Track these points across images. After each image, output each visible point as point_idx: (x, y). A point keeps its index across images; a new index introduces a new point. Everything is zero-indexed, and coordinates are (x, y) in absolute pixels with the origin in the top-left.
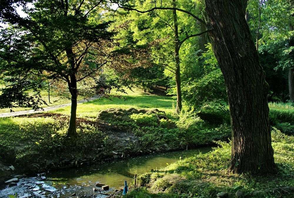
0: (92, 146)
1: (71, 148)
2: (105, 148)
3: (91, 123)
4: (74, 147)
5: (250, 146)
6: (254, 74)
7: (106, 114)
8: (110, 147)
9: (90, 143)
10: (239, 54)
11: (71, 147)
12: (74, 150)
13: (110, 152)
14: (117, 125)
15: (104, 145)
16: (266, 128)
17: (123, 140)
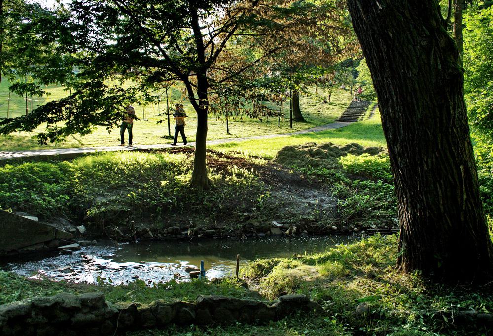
0: (233, 208)
1: (193, 208)
2: (259, 213)
3: (249, 166)
4: (199, 207)
5: (420, 213)
6: (410, 47)
7: (291, 152)
8: (272, 212)
9: (232, 203)
10: (377, 3)
11: (193, 205)
12: (197, 211)
13: (268, 222)
14: (305, 173)
15: (258, 208)
16: (453, 172)
17: (304, 203)
